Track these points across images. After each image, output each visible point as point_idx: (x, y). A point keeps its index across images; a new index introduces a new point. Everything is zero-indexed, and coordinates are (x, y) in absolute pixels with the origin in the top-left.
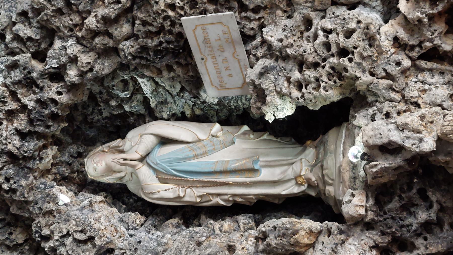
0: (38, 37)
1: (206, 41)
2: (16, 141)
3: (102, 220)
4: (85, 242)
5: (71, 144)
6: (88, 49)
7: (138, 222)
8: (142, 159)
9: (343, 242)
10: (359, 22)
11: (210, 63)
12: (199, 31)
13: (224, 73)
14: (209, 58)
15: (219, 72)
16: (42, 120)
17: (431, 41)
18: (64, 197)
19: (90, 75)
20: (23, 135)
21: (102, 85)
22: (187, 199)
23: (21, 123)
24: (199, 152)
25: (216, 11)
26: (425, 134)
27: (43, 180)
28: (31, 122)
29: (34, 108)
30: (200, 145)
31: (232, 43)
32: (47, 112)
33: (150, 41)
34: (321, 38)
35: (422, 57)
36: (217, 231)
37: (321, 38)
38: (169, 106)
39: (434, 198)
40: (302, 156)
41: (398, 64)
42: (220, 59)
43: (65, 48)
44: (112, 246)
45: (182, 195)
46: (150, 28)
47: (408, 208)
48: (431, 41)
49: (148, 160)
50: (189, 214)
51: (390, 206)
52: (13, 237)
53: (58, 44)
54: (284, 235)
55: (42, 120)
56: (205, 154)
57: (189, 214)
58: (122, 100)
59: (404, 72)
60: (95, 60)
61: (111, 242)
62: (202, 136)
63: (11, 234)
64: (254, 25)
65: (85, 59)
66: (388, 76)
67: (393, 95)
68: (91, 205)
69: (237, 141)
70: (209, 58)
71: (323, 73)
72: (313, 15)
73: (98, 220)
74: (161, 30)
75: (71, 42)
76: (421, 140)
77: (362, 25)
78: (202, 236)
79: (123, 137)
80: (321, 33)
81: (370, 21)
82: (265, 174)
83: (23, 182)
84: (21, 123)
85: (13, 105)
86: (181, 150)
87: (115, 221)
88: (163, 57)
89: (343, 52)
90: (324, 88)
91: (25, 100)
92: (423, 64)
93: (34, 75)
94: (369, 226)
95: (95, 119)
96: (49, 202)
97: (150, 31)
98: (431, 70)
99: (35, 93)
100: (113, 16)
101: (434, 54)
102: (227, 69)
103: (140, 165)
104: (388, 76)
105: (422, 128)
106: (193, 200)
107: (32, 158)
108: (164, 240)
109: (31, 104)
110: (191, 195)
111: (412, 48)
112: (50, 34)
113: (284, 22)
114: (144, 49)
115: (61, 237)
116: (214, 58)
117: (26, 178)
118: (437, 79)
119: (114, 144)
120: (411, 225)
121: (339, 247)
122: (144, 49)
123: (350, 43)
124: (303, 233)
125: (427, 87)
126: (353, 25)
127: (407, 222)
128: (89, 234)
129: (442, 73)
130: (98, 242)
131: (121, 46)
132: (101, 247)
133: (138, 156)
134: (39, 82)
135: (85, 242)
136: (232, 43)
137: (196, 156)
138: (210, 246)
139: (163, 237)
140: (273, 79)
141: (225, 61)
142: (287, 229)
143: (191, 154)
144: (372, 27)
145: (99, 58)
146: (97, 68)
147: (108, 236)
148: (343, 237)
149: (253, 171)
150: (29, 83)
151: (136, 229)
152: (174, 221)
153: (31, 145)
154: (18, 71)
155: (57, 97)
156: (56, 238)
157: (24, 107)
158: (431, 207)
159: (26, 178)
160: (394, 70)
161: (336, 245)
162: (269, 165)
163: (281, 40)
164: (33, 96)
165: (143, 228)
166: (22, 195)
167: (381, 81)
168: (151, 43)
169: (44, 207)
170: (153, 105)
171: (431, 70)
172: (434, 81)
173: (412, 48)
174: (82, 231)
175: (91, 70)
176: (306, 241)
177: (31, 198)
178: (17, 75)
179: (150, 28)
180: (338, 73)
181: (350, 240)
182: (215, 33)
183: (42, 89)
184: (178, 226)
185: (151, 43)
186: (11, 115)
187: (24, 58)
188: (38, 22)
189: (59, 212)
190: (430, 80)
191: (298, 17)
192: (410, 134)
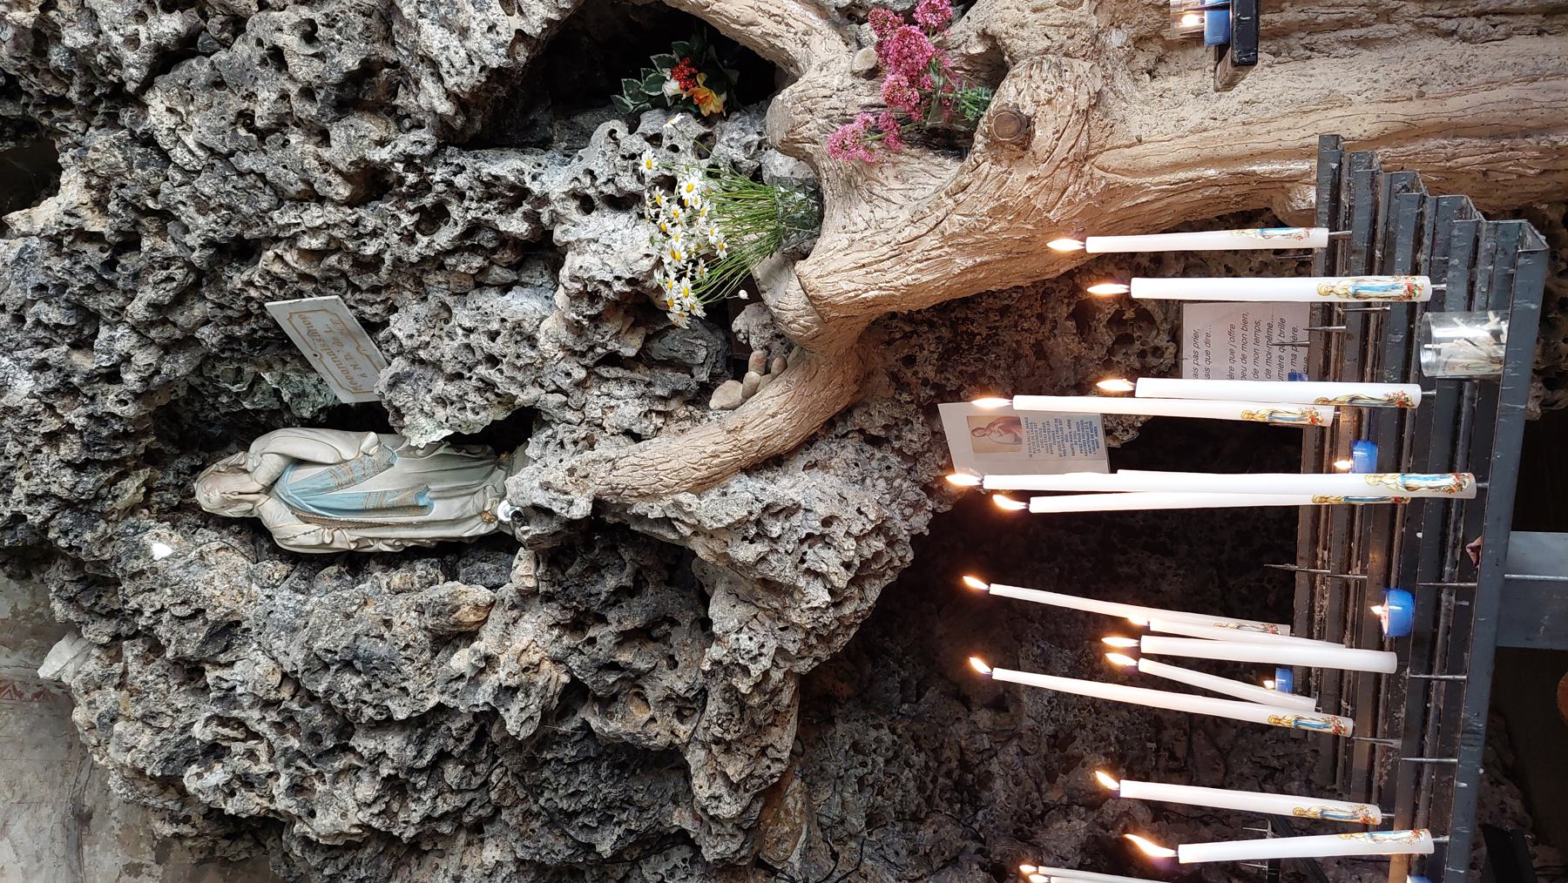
0: (73, 322)
1: (312, 333)
2: (67, 477)
3: (216, 583)
4: (193, 617)
5: (178, 456)
6: (145, 342)
7: (277, 576)
8: (268, 489)
9: (515, 621)
10: (503, 320)
11: (327, 360)
12: (296, 320)
13: (354, 373)
14: (324, 354)
15: (345, 372)
16: (105, 444)
17: (604, 346)
18: (161, 546)
19: (157, 379)
20: (78, 467)
21: (201, 375)
22: (337, 545)
23: (70, 449)
24: (344, 479)
25: (320, 294)
26: (575, 495)
27: (132, 520)
28: (86, 446)
29: (86, 427)
30: (345, 468)
31: (350, 334)
32: (105, 433)
33: (237, 328)
34: (460, 339)
35: (597, 364)
36: (385, 589)
37: (460, 339)
38: (311, 398)
39: (627, 557)
40: (488, 482)
41: (568, 375)
42: (341, 356)
43: (116, 340)
44: (235, 618)
45: (328, 540)
46: (230, 313)
47: (596, 569)
48: (604, 346)
49: (277, 488)
50: (355, 563)
51: (570, 571)
52: (104, 601)
53: (104, 332)
54: (440, 613)
55: (105, 444)
56: (352, 482)
57: (355, 563)
58: (238, 394)
59: (581, 385)
60: (161, 358)
61: (233, 612)
62: (348, 454)
63: (99, 597)
64: (378, 309)
65: (143, 358)
66: (559, 390)
67: (569, 415)
68: (202, 557)
69: (398, 461)
70: (324, 354)
71: (469, 385)
72: (450, 301)
73: (209, 583)
74: (247, 315)
75: (121, 330)
76: (571, 503)
77: (508, 325)
78: (353, 604)
79: (246, 448)
80: (460, 331)
81: (520, 317)
82: (439, 510)
83: (88, 536)
84: (70, 449)
85: (52, 424)
86: (314, 477)
87: (240, 579)
88: (264, 348)
89: (493, 360)
90: (473, 410)
91: (70, 417)
92: (603, 371)
93: (75, 380)
94: (548, 598)
95: (190, 428)
96: (137, 558)
97: (230, 318)
98: (617, 379)
99: (85, 405)
100: (167, 300)
101: (613, 359)
102: (355, 367)
103: (263, 498)
104: (559, 390)
105: (569, 488)
106: (345, 547)
107: (98, 497)
108: (308, 608)
109: (79, 423)
110: (344, 540)
111: (583, 355)
112: (93, 318)
113: (416, 308)
114: (231, 339)
115: (154, 613)
116: (331, 353)
117: (93, 529)
118: (626, 390)
119: (233, 460)
120: (599, 594)
121: (511, 627)
122: (231, 339)
123: (496, 348)
124: (467, 609)
125: (613, 403)
126: (495, 326)
127: (594, 591)
128: (195, 606)
129: (632, 382)
130: (211, 616)
131: (197, 335)
132: (216, 623)
133: (257, 487)
134: (84, 390)
135: (193, 617)
136: (350, 334)
137: (340, 486)
138: (361, 620)
139: (305, 603)
140: (410, 392)
141: (348, 357)
142: (445, 604)
143: (333, 482)
144: (525, 324)
145: (167, 353)
146: (166, 368)
147: (227, 604)
148: (515, 613)
149: (416, 508)
150: (68, 390)
151: (274, 586)
152: (333, 570)
153: (89, 482)
154: (50, 373)
155: (118, 410)
156: (147, 614)
157: (70, 427)
158: (622, 568)
159: (93, 529)
160: (565, 383)
161: (507, 624)
162: (444, 495)
163: (411, 336)
164: (81, 410)
165: (285, 585)
166: (90, 553)
167: (550, 397)
168: (239, 331)
169: (128, 568)
170: (286, 399)
171: (617, 379)
172: (622, 393)
173: (583, 355)
174: (184, 603)
175: (157, 372)
176: (472, 618)
177: (107, 556)
178: (50, 380)
179: (230, 313)
180: (487, 386)
181: (526, 617)
182: (321, 322)
183: (93, 399)
184: (339, 576)
185: (239, 331)
186: (53, 438)
187: (54, 354)
188: (66, 300)
189: (155, 571)
190: (617, 393)
191: (433, 301)
192: (556, 495)
